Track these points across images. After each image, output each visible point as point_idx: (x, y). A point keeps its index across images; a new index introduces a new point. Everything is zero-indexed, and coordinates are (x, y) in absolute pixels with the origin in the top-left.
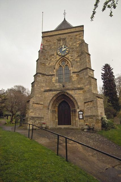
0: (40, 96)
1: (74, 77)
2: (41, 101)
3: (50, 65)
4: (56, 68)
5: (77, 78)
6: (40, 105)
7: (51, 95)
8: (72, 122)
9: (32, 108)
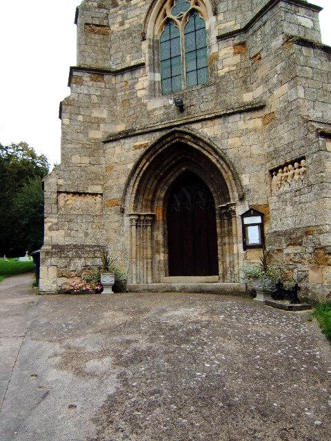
0: (86, 160)
1: (227, 58)
2: (95, 178)
3: (127, 26)
4: (149, 35)
5: (238, 58)
6: (89, 199)
7: (126, 155)
8: (220, 263)
9: (55, 210)
